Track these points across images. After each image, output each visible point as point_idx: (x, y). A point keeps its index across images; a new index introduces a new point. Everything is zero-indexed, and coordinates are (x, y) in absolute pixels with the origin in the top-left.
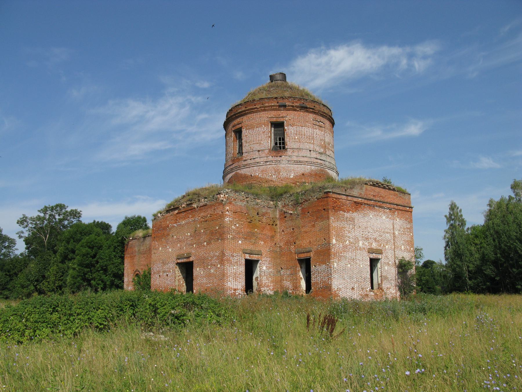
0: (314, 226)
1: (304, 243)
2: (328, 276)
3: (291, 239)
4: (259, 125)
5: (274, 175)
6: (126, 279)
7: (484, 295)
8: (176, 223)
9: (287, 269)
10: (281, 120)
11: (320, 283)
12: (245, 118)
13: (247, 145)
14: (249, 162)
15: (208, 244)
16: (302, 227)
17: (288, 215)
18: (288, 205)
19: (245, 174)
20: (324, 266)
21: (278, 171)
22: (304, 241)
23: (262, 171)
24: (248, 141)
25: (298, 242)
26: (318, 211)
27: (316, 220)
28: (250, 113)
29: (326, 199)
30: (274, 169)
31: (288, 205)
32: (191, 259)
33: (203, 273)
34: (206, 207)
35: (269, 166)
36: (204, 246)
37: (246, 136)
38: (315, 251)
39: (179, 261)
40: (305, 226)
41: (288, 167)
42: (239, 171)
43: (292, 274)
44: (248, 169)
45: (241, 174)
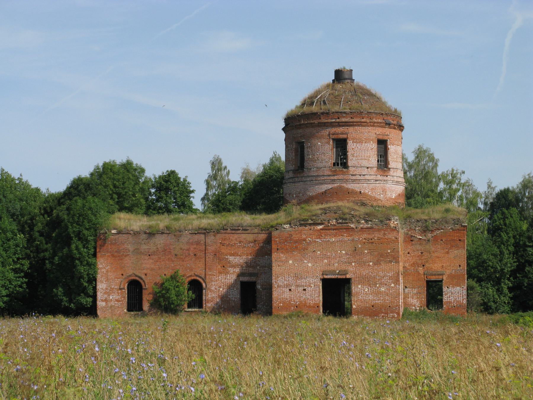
0: (448, 253)
1: (436, 267)
2: (463, 297)
3: (420, 262)
4: (367, 140)
5: (382, 194)
6: (101, 286)
7: (54, 317)
8: (319, 238)
9: (414, 287)
10: (385, 138)
11: (454, 302)
12: (351, 129)
13: (354, 159)
14: (358, 177)
15: (375, 264)
16: (434, 252)
17: (416, 240)
18: (415, 230)
19: (353, 190)
20: (458, 288)
21: (384, 191)
22: (436, 265)
23: (372, 189)
24: (355, 155)
25: (427, 265)
26: (453, 240)
27: (450, 248)
28: (359, 126)
29: (462, 231)
30: (382, 188)
31: (415, 230)
32: (348, 276)
33: (368, 290)
34: (371, 230)
35: (378, 185)
36: (369, 265)
37: (353, 149)
38: (448, 275)
39: (326, 277)
40: (436, 252)
41: (391, 187)
42: (345, 185)
43: (419, 293)
44: (358, 185)
45: (347, 188)
